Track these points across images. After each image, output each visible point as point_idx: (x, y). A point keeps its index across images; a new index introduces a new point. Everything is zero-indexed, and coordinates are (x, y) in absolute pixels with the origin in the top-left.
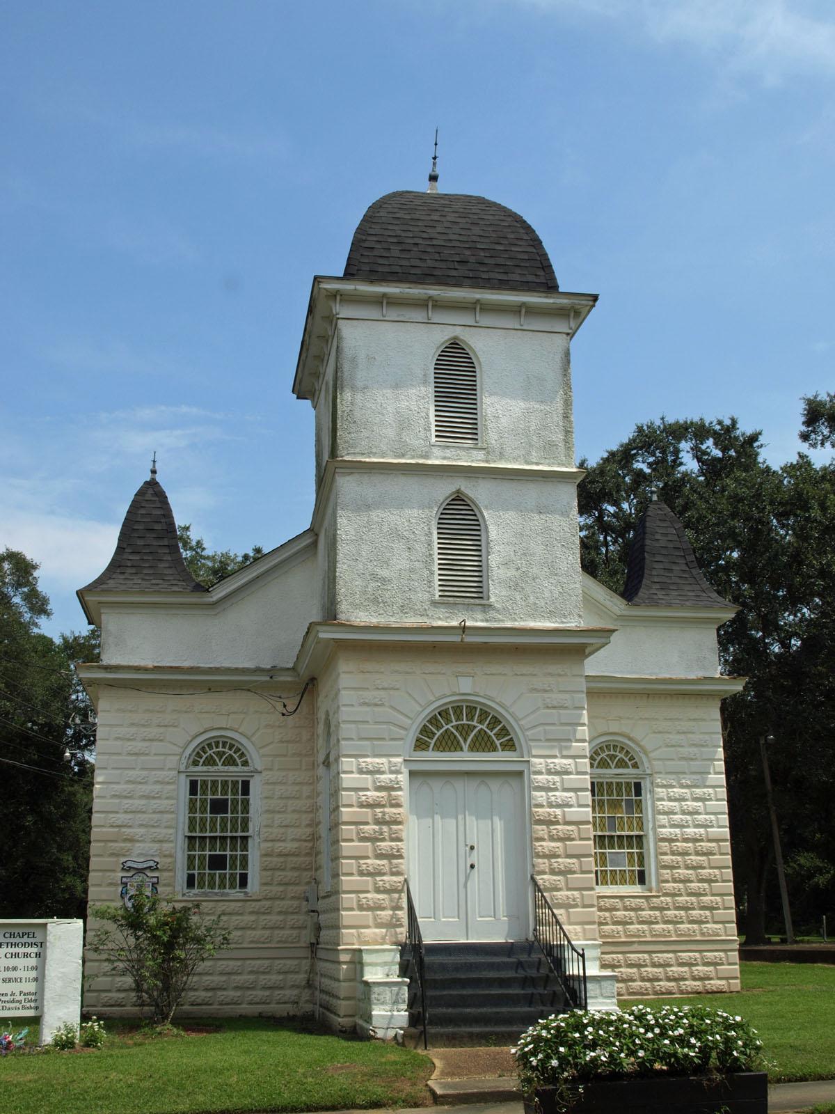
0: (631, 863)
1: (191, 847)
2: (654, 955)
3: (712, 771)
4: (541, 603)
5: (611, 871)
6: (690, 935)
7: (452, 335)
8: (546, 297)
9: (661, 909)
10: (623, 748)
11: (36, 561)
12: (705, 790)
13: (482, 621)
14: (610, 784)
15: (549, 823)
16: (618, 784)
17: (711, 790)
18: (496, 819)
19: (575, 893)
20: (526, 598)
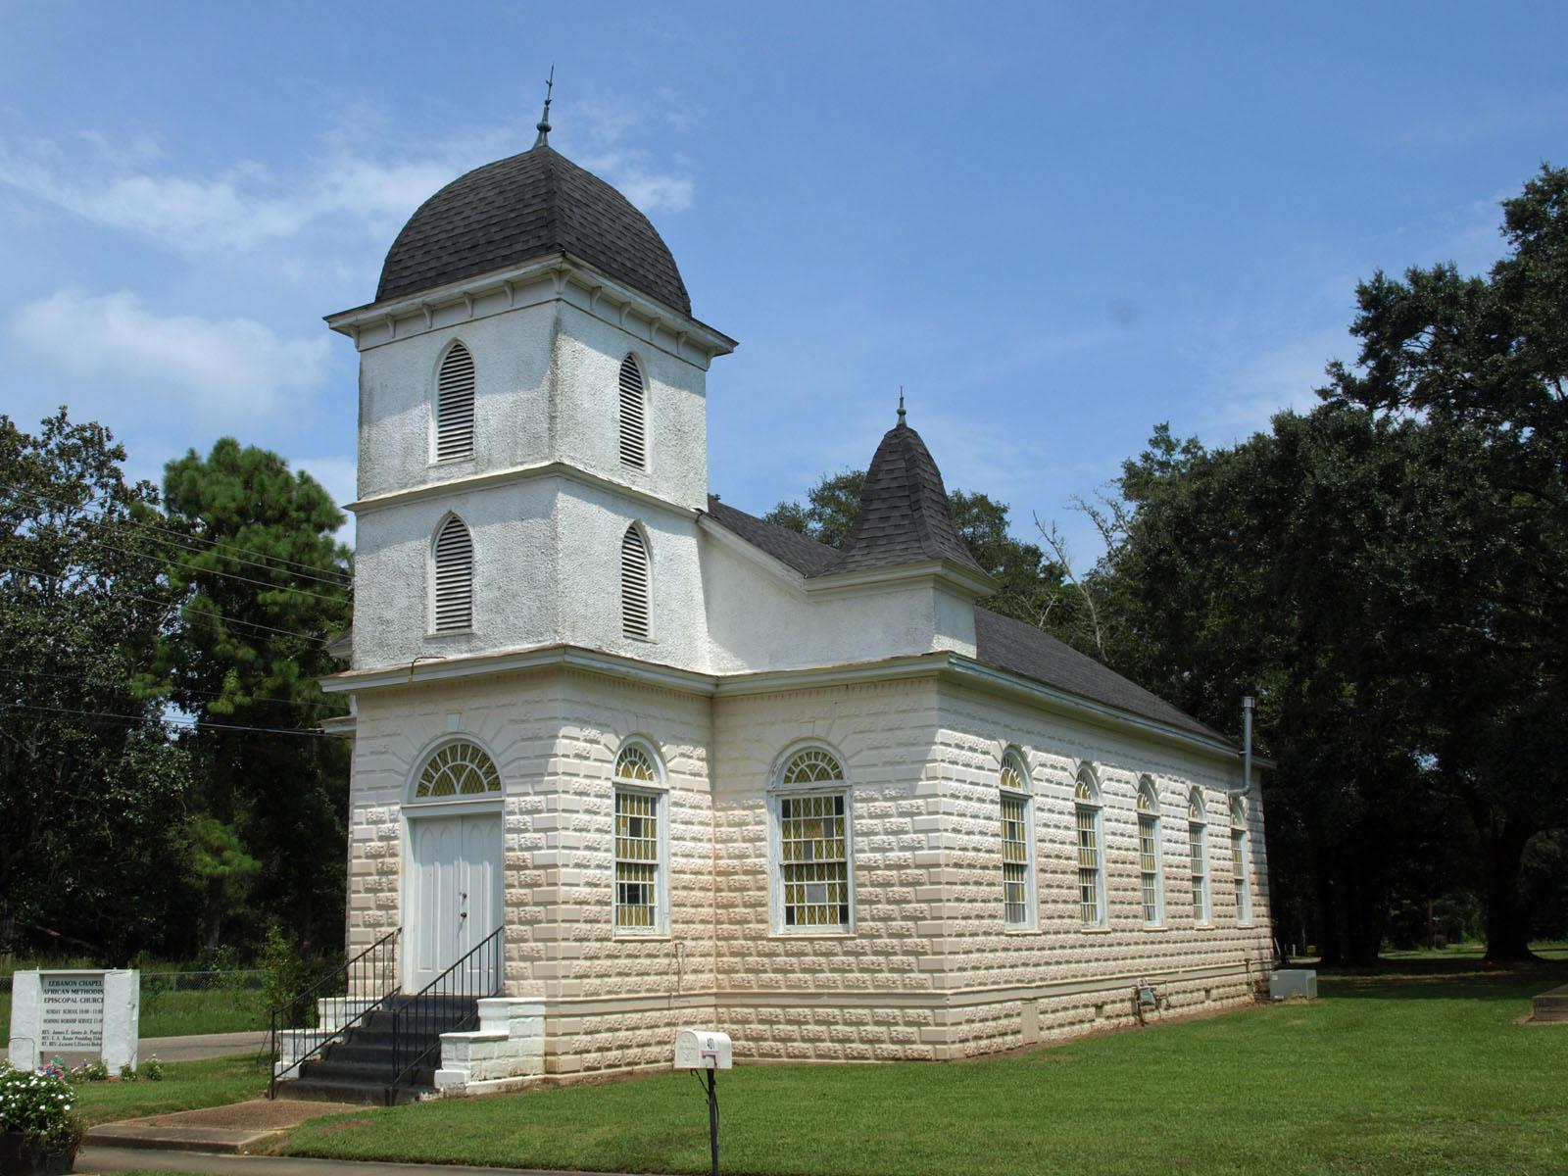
0: (832, 898)
1: (788, 878)
2: (846, 1011)
3: (923, 776)
4: (519, 623)
5: (809, 907)
6: (889, 987)
7: (450, 338)
8: (517, 269)
9: (856, 954)
10: (825, 755)
11: (1003, 503)
12: (913, 802)
13: (467, 652)
14: (807, 801)
15: (519, 868)
16: (816, 800)
17: (920, 802)
18: (487, 864)
19: (539, 944)
20: (506, 619)
